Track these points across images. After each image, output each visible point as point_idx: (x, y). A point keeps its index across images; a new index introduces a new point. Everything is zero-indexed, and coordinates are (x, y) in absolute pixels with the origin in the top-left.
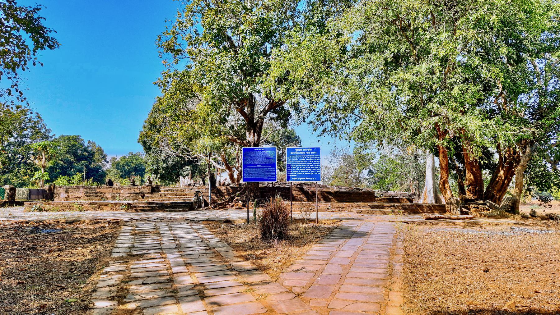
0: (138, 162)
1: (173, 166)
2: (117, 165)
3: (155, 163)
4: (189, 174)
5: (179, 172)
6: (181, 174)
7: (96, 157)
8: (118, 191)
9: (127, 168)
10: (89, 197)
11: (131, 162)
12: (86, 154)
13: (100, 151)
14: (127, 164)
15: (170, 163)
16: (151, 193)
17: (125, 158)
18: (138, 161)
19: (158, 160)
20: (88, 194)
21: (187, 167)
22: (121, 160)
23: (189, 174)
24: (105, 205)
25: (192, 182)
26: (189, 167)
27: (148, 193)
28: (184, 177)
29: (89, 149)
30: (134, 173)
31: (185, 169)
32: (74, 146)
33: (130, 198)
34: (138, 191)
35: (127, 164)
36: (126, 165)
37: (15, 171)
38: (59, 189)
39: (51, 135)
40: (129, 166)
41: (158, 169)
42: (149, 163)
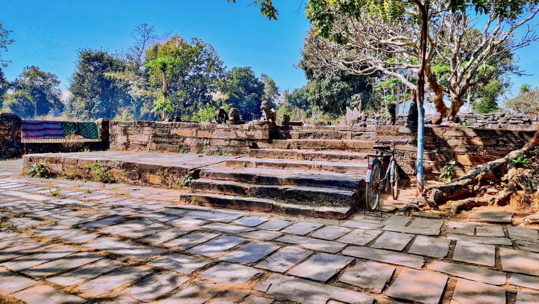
1: (340, 94)
3: (317, 91)
4: (359, 103)
5: (345, 102)
6: (349, 105)
8: (206, 134)
10: (160, 145)
11: (303, 95)
12: (256, 86)
13: (272, 84)
14: (298, 97)
15: (335, 90)
16: (270, 141)
17: (296, 90)
21: (357, 95)
22: (294, 93)
23: (359, 103)
25: (362, 115)
26: (359, 96)
27: (262, 140)
28: (352, 109)
29: (260, 80)
31: (353, 97)
32: (245, 77)
33: (229, 149)
34: (242, 135)
35: (298, 97)
37: (194, 103)
38: (114, 127)
39: (223, 67)
40: (300, 99)
41: (321, 98)
42: (311, 91)
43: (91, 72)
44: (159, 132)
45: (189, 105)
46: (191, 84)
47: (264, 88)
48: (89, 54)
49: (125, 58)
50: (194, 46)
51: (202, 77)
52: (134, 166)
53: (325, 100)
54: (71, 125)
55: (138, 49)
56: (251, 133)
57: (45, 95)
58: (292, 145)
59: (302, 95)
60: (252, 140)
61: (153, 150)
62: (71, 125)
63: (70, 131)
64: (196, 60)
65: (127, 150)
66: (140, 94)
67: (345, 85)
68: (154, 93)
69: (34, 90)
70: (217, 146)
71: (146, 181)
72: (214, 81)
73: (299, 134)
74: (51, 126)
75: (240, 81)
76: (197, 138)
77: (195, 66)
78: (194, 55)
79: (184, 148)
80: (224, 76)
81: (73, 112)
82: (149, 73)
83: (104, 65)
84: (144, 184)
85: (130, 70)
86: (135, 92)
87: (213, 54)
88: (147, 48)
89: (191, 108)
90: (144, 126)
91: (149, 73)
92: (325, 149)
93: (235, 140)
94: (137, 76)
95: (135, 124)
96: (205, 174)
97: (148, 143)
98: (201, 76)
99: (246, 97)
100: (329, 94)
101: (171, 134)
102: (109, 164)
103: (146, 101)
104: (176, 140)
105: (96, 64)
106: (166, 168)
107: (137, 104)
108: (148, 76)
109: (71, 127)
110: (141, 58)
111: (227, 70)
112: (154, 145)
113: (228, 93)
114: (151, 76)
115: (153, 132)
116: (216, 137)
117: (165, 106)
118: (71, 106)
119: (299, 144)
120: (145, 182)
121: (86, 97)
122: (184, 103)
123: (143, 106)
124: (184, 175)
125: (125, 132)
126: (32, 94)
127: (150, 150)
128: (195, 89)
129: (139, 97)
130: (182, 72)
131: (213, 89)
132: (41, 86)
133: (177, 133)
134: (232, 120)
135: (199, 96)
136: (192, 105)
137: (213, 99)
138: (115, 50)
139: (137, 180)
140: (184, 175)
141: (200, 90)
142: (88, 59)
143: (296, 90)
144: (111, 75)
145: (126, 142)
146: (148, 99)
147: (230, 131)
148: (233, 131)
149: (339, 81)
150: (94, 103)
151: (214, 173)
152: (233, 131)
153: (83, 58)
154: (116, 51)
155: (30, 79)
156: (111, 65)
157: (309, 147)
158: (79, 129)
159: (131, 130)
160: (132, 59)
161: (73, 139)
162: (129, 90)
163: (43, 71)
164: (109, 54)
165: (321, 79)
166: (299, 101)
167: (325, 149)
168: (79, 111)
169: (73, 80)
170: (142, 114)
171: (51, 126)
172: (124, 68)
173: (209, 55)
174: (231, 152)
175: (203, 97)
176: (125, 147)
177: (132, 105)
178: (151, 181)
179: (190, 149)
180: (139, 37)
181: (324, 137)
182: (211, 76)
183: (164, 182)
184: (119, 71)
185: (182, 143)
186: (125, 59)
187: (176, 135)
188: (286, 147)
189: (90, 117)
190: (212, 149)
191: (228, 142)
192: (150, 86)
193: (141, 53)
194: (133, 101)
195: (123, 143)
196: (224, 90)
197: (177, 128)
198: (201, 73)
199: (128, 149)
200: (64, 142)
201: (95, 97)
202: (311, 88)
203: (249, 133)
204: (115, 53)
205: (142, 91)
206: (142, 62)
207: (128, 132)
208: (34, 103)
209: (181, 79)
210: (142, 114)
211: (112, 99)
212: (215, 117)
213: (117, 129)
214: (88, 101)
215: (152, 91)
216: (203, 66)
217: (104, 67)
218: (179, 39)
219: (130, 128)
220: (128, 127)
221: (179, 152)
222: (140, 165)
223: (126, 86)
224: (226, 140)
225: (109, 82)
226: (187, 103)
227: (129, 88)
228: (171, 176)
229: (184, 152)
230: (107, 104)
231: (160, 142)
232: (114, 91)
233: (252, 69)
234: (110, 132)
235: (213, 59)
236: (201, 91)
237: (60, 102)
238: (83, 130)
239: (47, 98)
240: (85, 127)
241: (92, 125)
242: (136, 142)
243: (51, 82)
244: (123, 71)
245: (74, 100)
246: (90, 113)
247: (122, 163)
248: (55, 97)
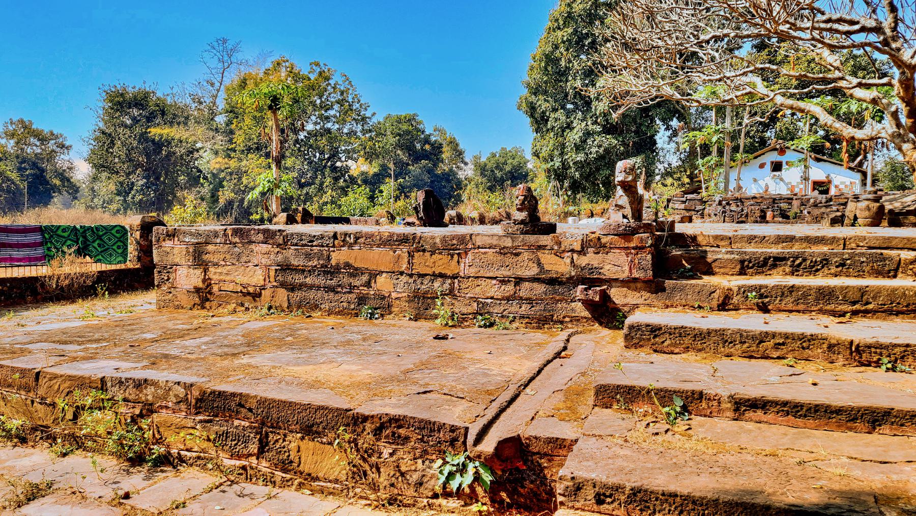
0: (515, 162)
1: (601, 158)
2: (482, 169)
3: (556, 153)
7: (446, 154)
8: (441, 263)
9: (499, 174)
10: (297, 296)
11: (505, 163)
12: (427, 147)
13: (453, 144)
16: (655, 286)
17: (494, 155)
18: (516, 160)
19: (563, 146)
20: (291, 278)
22: (488, 159)
24: (309, 431)
27: (629, 283)
29: (433, 139)
30: (509, 182)
32: (408, 132)
33: (514, 307)
34: (561, 267)
36: (497, 168)
37: (317, 181)
38: (168, 244)
39: (368, 114)
40: (501, 170)
41: (565, 166)
43: (126, 126)
44: (296, 256)
45: (309, 184)
46: (311, 146)
47: (441, 152)
48: (122, 95)
49: (188, 101)
50: (313, 77)
51: (330, 133)
52: (241, 405)
53: (573, 170)
54: (66, 234)
55: (212, 85)
56: (590, 259)
57: (43, 171)
58: (735, 300)
59: (503, 164)
60: (591, 283)
61: (280, 309)
62: (66, 234)
63: (65, 249)
64: (318, 102)
65: (203, 308)
66: (217, 166)
67: (610, 141)
68: (244, 163)
69: (23, 161)
70: (475, 299)
71: (285, 466)
72: (353, 140)
73: (742, 262)
74: (15, 238)
75: (399, 140)
76: (411, 276)
77: (317, 113)
78: (314, 93)
79: (373, 303)
80: (370, 131)
81: (96, 200)
82: (233, 126)
83: (152, 113)
84: (279, 474)
85: (199, 123)
86: (208, 162)
87: (350, 92)
88: (227, 82)
89: (312, 190)
90: (251, 242)
91: (233, 126)
92: (867, 312)
93: (533, 280)
94: (211, 134)
95: (225, 235)
96: (590, 493)
97: (263, 288)
98: (329, 131)
99: (410, 167)
100: (581, 157)
101: (333, 262)
102: (149, 394)
103: (228, 178)
104: (346, 280)
105: (135, 112)
106: (365, 419)
107: (211, 183)
108: (232, 132)
109: (67, 238)
110: (218, 101)
111: (375, 120)
112: (282, 294)
113: (380, 161)
114: (237, 133)
115: (280, 258)
116: (472, 272)
117: (277, 186)
118: (93, 190)
119: (761, 296)
120: (285, 471)
121: (117, 173)
122: (299, 182)
123: (223, 187)
124: (442, 453)
125: (199, 258)
126: (20, 169)
127: (270, 308)
128: (318, 155)
129: (215, 171)
130: (293, 125)
131: (349, 154)
132: (36, 155)
133: (351, 262)
134: (522, 222)
135: (325, 167)
136: (314, 183)
137: (351, 173)
138: (173, 85)
139: (254, 460)
140: (442, 453)
141: (326, 156)
142: (119, 103)
143: (494, 155)
144: (163, 132)
145: (201, 285)
146: (231, 174)
147: (517, 255)
148: (526, 255)
149: (599, 133)
150: (133, 183)
151: (635, 492)
152: (526, 255)
153: (111, 101)
154: (172, 89)
155: (17, 143)
156: (163, 113)
157: (801, 307)
158: (85, 240)
159: (213, 252)
160: (201, 103)
161: (70, 266)
162: (196, 159)
163: (40, 128)
164: (159, 94)
165: (563, 131)
166: (499, 174)
167: (867, 312)
168: (107, 199)
169: (92, 142)
170: (222, 201)
171: (15, 238)
172: (187, 118)
173: (342, 93)
174: (522, 317)
175: (334, 169)
176: (197, 300)
177: (202, 185)
178: (305, 467)
179: (390, 306)
180: (214, 63)
181: (833, 270)
182: (345, 131)
183: (358, 474)
184: (179, 124)
185: (365, 290)
186: (188, 103)
187: (348, 265)
188: (715, 303)
189: (125, 209)
190: (461, 308)
191: (510, 288)
192: (235, 151)
193: (218, 90)
194: (205, 178)
195: (191, 287)
196: (370, 156)
197: (351, 246)
198: (329, 125)
199: (207, 304)
200: (50, 273)
201: (134, 172)
202: (544, 149)
203: (583, 261)
204: (169, 91)
205: (219, 159)
206: (220, 108)
207: (205, 257)
208: (24, 186)
209: (292, 136)
210: (222, 201)
211: (166, 175)
212: (416, 209)
213: (176, 251)
214: (121, 179)
215: (240, 160)
216: (332, 112)
217: (150, 118)
218: (287, 64)
219: (210, 248)
220: (207, 243)
221: (357, 315)
222: (263, 402)
223: (192, 152)
224: (504, 281)
225: (158, 145)
226: (303, 181)
227: (196, 155)
228: (386, 452)
229: (372, 314)
230: (157, 185)
231: (301, 286)
232: (169, 160)
233: (419, 119)
234: (156, 259)
235: (350, 100)
236: (329, 159)
237: (71, 183)
238: (96, 245)
239: (48, 177)
240: (100, 237)
241: (118, 232)
242: (231, 287)
243: (55, 147)
244: (186, 124)
245: (95, 179)
246: (125, 201)
247: (196, 393)
248: (62, 174)
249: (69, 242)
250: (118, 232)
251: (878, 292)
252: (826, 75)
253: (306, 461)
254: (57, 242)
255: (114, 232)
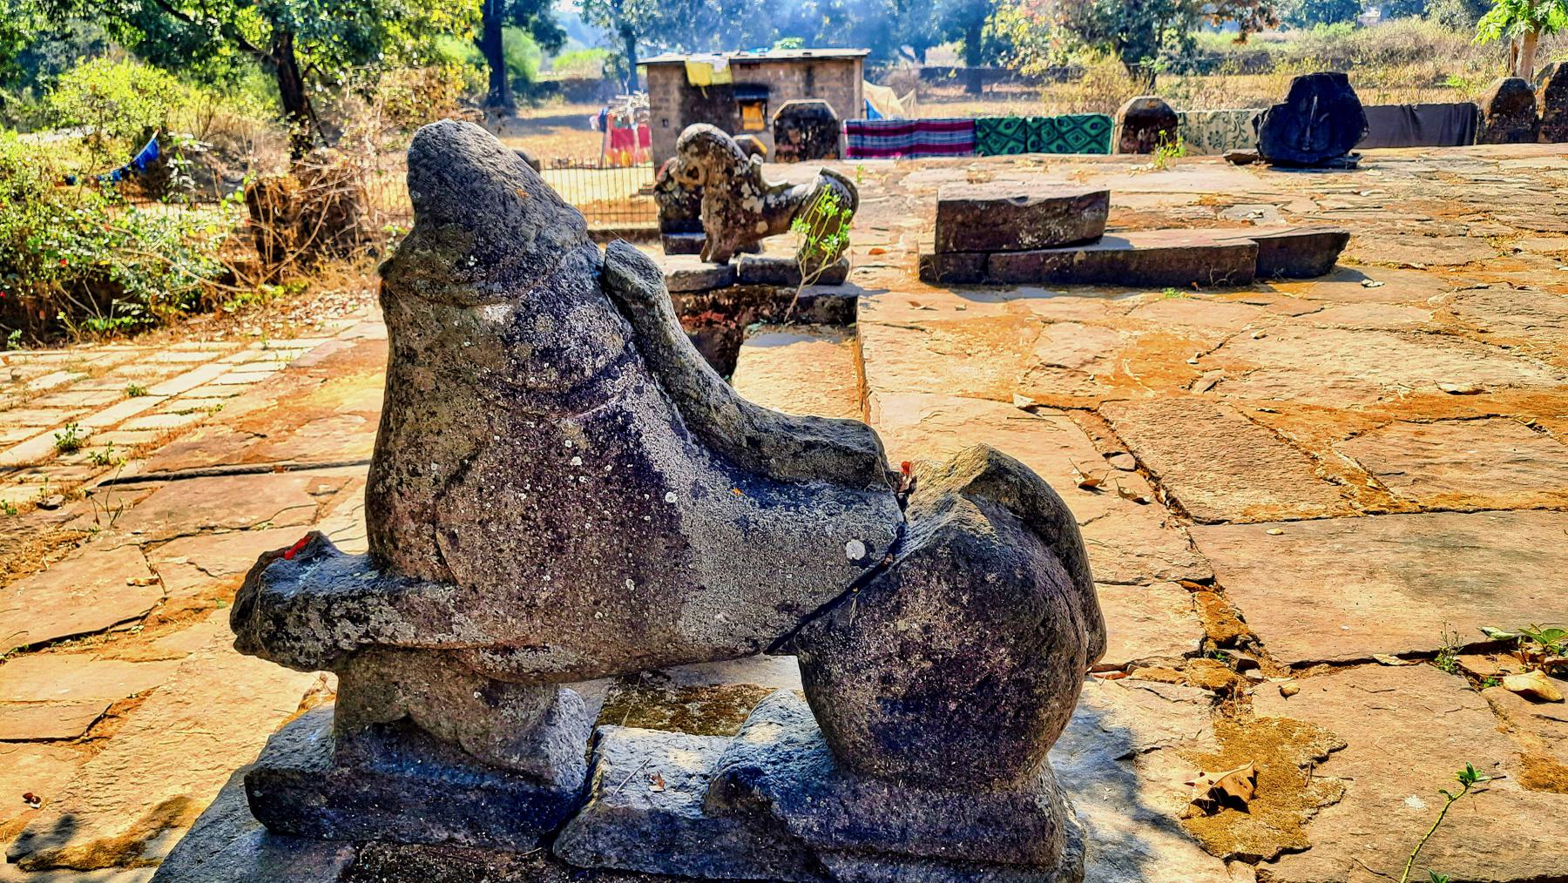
54: (1009, 132)
62: (1009, 132)
241: (1093, 126)
249: (1012, 144)
250: (1093, 126)
251: (611, 222)
252: (174, 443)
253: (1472, 403)
254: (996, 142)
255: (1087, 126)
